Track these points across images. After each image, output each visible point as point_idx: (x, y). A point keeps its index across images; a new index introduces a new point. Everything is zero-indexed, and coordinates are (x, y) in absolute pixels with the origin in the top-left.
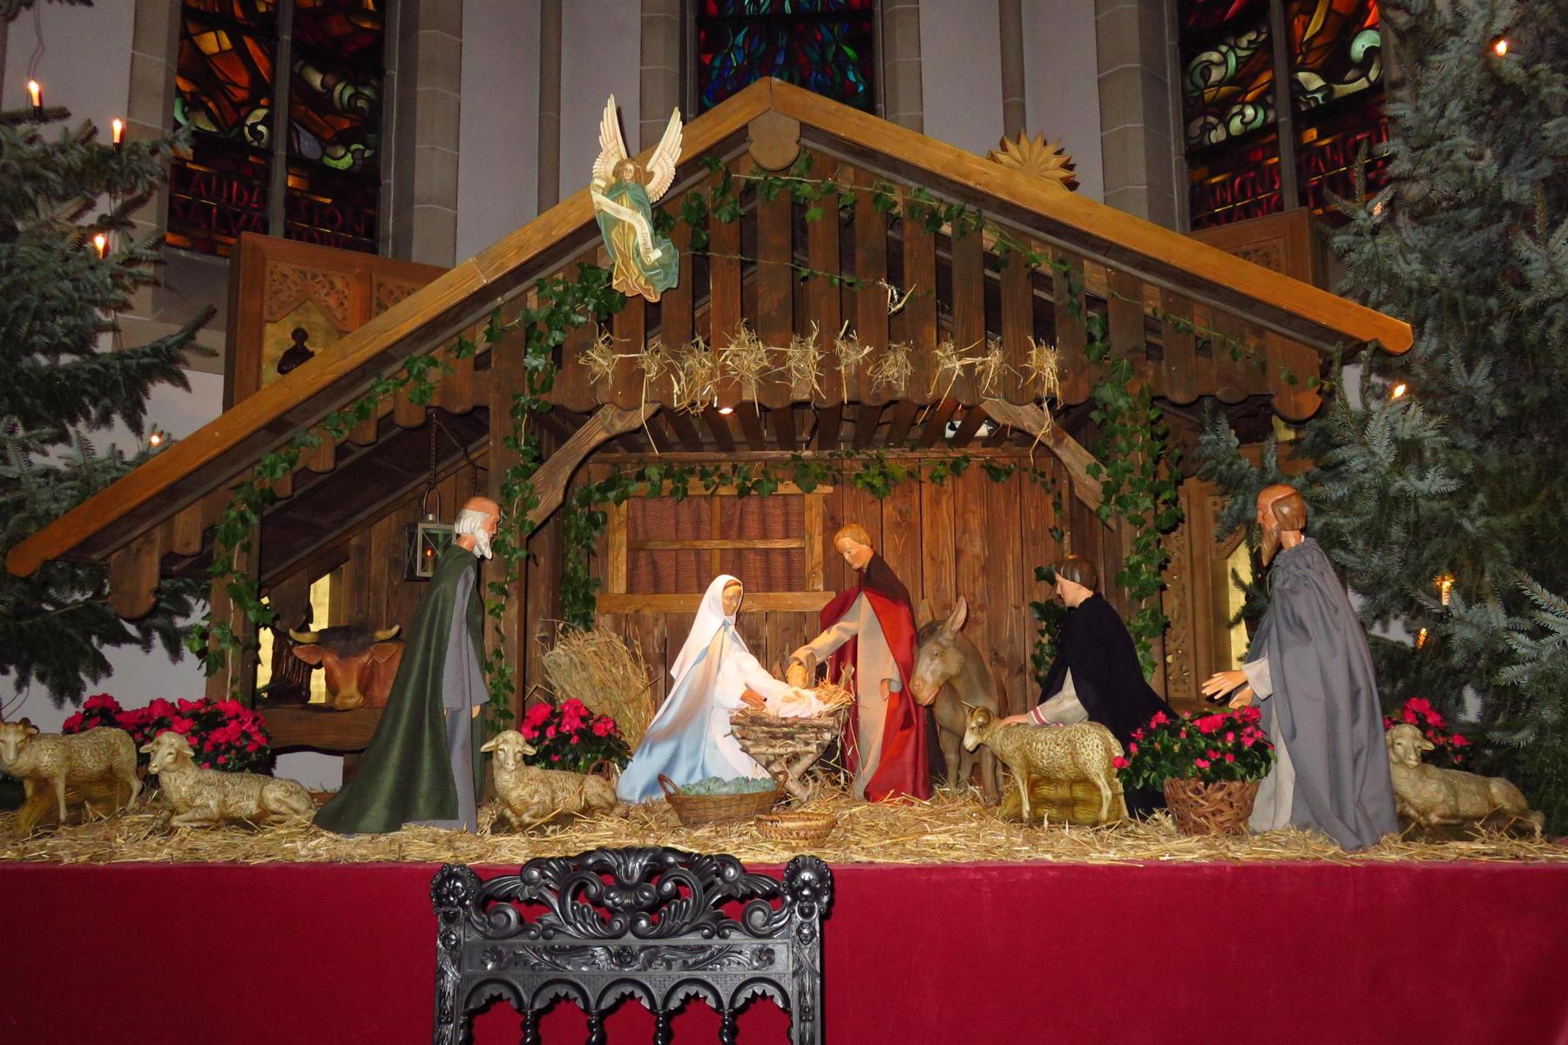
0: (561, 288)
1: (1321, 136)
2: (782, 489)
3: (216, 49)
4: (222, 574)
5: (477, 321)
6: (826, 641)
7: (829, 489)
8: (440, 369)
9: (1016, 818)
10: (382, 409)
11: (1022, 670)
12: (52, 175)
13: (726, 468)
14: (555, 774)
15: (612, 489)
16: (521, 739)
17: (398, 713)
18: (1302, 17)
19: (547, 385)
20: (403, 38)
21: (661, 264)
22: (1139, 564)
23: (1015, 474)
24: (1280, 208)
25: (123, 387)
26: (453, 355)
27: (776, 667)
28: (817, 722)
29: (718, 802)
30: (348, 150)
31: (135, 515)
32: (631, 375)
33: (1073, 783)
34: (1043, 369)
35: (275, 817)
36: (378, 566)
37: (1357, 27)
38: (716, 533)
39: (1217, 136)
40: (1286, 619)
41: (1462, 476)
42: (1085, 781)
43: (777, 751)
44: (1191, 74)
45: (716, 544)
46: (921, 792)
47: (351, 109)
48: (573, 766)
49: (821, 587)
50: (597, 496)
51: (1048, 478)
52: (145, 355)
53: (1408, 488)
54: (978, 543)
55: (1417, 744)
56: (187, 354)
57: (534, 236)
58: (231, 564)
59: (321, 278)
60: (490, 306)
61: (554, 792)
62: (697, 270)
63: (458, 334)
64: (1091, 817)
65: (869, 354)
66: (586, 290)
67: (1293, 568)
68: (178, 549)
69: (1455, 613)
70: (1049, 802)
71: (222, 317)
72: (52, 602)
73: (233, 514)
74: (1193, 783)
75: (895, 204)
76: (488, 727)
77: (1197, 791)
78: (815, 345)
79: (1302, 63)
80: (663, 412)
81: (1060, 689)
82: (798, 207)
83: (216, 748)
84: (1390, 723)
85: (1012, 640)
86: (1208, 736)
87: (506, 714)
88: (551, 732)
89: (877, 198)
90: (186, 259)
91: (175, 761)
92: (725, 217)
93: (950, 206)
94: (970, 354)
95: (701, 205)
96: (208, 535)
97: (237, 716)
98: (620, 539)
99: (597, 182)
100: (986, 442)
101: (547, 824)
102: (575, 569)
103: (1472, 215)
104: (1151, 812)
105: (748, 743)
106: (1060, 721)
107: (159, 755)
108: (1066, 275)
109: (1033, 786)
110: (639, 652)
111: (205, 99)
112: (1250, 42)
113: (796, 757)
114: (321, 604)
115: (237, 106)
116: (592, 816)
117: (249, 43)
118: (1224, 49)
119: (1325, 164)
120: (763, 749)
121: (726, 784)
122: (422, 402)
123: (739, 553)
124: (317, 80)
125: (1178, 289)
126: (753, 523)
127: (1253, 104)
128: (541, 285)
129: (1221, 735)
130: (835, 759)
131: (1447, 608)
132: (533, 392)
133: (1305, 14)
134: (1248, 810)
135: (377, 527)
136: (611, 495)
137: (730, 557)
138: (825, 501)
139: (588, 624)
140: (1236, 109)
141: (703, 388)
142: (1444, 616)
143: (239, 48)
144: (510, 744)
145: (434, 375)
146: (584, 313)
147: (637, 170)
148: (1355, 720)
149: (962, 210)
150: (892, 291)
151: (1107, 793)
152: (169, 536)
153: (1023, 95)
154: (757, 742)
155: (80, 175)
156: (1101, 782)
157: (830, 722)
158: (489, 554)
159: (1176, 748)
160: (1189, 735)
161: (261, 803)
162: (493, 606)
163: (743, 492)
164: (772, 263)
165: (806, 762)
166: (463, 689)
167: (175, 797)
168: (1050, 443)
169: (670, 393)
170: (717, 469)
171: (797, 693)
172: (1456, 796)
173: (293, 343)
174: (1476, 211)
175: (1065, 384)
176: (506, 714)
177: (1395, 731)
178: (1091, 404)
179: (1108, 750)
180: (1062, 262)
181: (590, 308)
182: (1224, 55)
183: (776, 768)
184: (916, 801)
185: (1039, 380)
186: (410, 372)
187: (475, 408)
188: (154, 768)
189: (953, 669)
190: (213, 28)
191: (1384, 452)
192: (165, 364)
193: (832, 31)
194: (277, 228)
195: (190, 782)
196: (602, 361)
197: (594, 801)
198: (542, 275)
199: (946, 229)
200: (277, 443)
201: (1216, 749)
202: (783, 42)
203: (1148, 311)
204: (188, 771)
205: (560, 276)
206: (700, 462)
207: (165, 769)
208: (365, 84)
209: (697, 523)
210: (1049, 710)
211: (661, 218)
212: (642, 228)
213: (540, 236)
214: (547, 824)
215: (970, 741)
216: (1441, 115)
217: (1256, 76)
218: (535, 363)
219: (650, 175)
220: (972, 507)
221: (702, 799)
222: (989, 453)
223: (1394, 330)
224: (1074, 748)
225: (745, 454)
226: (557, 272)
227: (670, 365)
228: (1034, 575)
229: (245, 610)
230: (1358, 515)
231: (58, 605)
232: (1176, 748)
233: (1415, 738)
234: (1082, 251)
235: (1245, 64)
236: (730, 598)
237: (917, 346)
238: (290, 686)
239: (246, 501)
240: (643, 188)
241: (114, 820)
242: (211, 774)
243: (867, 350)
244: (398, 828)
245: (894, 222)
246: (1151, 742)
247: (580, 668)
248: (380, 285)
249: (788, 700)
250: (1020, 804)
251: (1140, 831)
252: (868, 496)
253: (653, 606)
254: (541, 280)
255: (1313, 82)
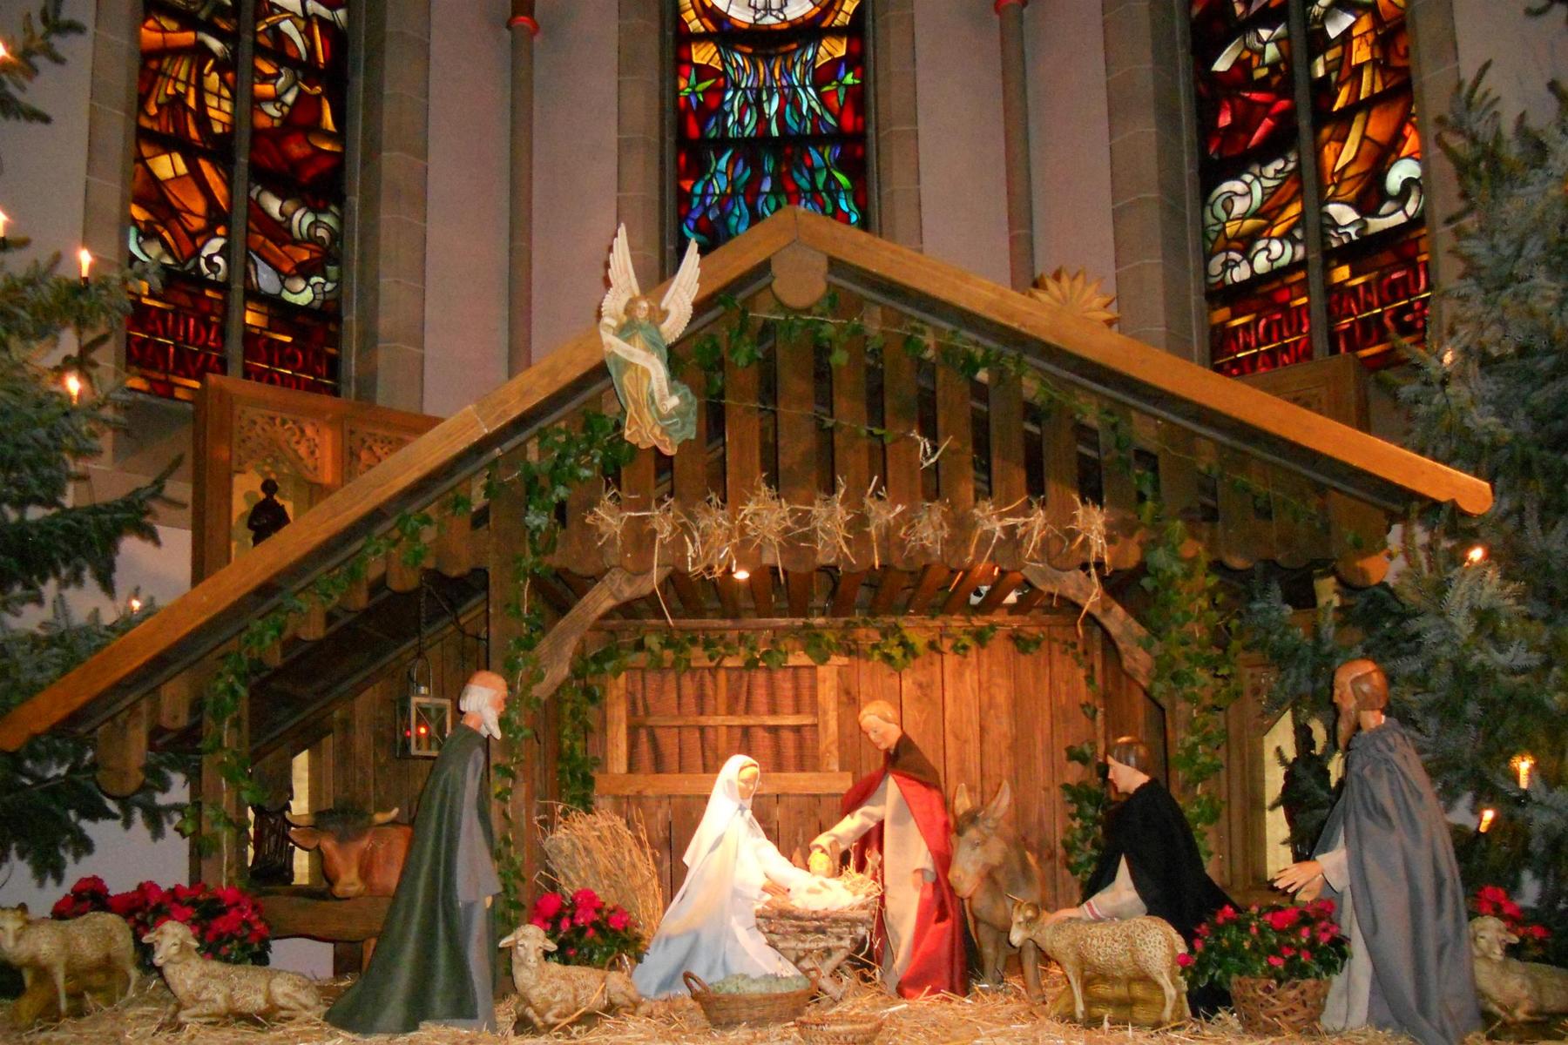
0: (562, 438)
1: (1354, 275)
2: (792, 661)
3: (170, 174)
4: (212, 751)
5: (476, 473)
6: (850, 826)
7: (844, 660)
8: (435, 528)
9: (1068, 1017)
10: (373, 571)
11: (1052, 856)
12: (22, 313)
13: (732, 635)
14: (574, 970)
15: (609, 659)
16: (542, 933)
17: (411, 904)
18: (1333, 145)
19: (550, 545)
20: (364, 164)
21: (679, 412)
22: (1195, 745)
23: (1044, 645)
24: (1308, 354)
25: (90, 544)
26: (449, 512)
27: (797, 855)
28: (850, 915)
29: (750, 1002)
30: (308, 284)
31: (122, 687)
32: (641, 537)
33: (1130, 981)
34: (1090, 531)
35: (284, 1013)
36: (362, 740)
37: (1393, 156)
38: (722, 708)
39: (1240, 274)
40: (1365, 804)
41: (1540, 649)
42: (1146, 979)
43: (807, 946)
44: (1212, 205)
45: (721, 720)
46: (957, 985)
47: (311, 239)
48: (587, 961)
49: (836, 767)
50: (593, 668)
51: (1080, 648)
52: (117, 509)
53: (1488, 663)
54: (1005, 720)
55: (1502, 936)
56: (155, 505)
57: (533, 387)
58: (221, 740)
59: (290, 424)
60: (485, 459)
61: (576, 990)
62: (714, 418)
63: (452, 489)
64: (1153, 1017)
65: (902, 513)
66: (591, 441)
67: (1373, 751)
68: (166, 722)
69: (1534, 797)
70: (1106, 1002)
71: (187, 468)
72: (31, 775)
73: (221, 686)
74: (1264, 982)
75: (927, 347)
76: (502, 922)
77: (1268, 990)
78: (842, 503)
79: (1334, 194)
80: (676, 581)
81: (1112, 878)
82: (821, 352)
83: (219, 937)
84: (1472, 915)
85: (1041, 823)
86: (1280, 932)
87: (519, 906)
88: (565, 925)
89: (908, 340)
90: (143, 403)
91: (180, 952)
92: (742, 361)
93: (987, 350)
94: (1011, 514)
95: (715, 347)
96: (197, 707)
97: (237, 904)
98: (619, 715)
99: (606, 320)
100: (1013, 609)
101: (572, 1024)
102: (572, 747)
103: (1546, 364)
104: (1214, 1011)
105: (775, 937)
106: (1117, 915)
107: (163, 947)
108: (1114, 427)
109: (1087, 984)
110: (644, 837)
111: (160, 228)
112: (1277, 172)
113: (828, 952)
114: (300, 780)
115: (193, 236)
116: (616, 1015)
117: (205, 166)
118: (1248, 178)
119: (1358, 305)
120: (793, 944)
121: (754, 981)
122: (416, 563)
123: (746, 729)
124: (274, 206)
125: (1237, 444)
126: (760, 696)
127: (1280, 238)
128: (542, 435)
129: (1294, 930)
130: (866, 959)
131: (1526, 791)
132: (535, 553)
133: (1337, 140)
134: (1320, 1008)
135: (362, 698)
136: (608, 666)
137: (738, 734)
138: (839, 674)
139: (587, 806)
140: (1261, 244)
141: (720, 552)
142: (1523, 799)
143: (195, 173)
144: (531, 940)
145: (429, 534)
146: (589, 465)
147: (651, 309)
148: (1439, 911)
149: (1000, 355)
150: (925, 444)
151: (1170, 991)
152: (155, 710)
153: (1031, 228)
154: (784, 935)
155: (49, 312)
156: (1165, 981)
157: (865, 914)
158: (498, 734)
159: (1246, 945)
160: (1260, 930)
161: (269, 998)
162: (498, 789)
163: (751, 664)
164: (795, 411)
165: (838, 957)
166: (476, 882)
167: (181, 991)
168: (1097, 612)
169: (684, 557)
170: (722, 638)
171: (823, 884)
172: (1540, 991)
173: (262, 496)
174: (1552, 359)
175: (1115, 548)
176: (519, 906)
177: (1479, 923)
178: (1142, 569)
179: (1172, 947)
180: (1110, 413)
181: (597, 461)
182: (1249, 185)
183: (806, 964)
184: (956, 998)
185: (1086, 545)
186: (403, 531)
187: (475, 571)
188: (158, 959)
189: (996, 857)
190: (167, 150)
191: (1463, 625)
192: (134, 517)
193: (822, 155)
194: (236, 368)
195: (195, 974)
196: (609, 519)
197: (618, 999)
198: (544, 423)
199: (982, 375)
200: (264, 608)
201: (1290, 945)
202: (769, 165)
203: (1203, 467)
204: (193, 962)
205: (563, 425)
206: (704, 630)
207: (170, 961)
208: (325, 211)
209: (701, 697)
210: (1103, 900)
211: (676, 359)
212: (658, 372)
213: (547, 380)
214: (572, 1024)
215: (1016, 937)
216: (1519, 255)
217: (1282, 208)
218: (537, 522)
219: (665, 314)
220: (999, 681)
221: (734, 999)
222: (1015, 622)
223: (1469, 490)
224: (1133, 944)
225: (751, 621)
226: (558, 420)
227: (684, 525)
228: (1064, 754)
229: (240, 789)
230: (1434, 692)
231: (40, 780)
232: (1246, 945)
233: (1499, 930)
234: (1131, 401)
235: (1272, 194)
236: (746, 781)
237: (953, 505)
238: (273, 871)
239: (234, 672)
240: (657, 328)
241: (117, 1016)
242: (215, 966)
243: (899, 508)
244: (416, 1028)
245: (926, 369)
246: (1218, 938)
247: (590, 849)
248: (352, 432)
249: (811, 891)
250: (1072, 1003)
251: (1207, 1032)
252: (886, 669)
253: (653, 785)
254: (541, 430)
255: (1344, 214)
